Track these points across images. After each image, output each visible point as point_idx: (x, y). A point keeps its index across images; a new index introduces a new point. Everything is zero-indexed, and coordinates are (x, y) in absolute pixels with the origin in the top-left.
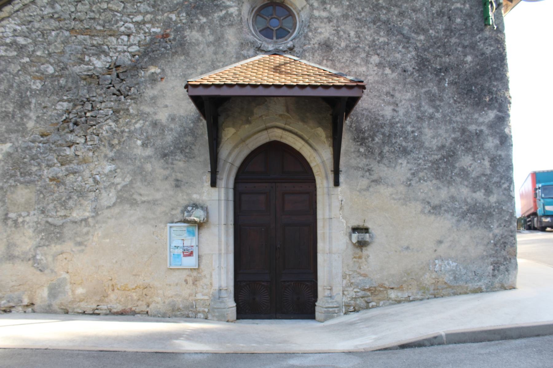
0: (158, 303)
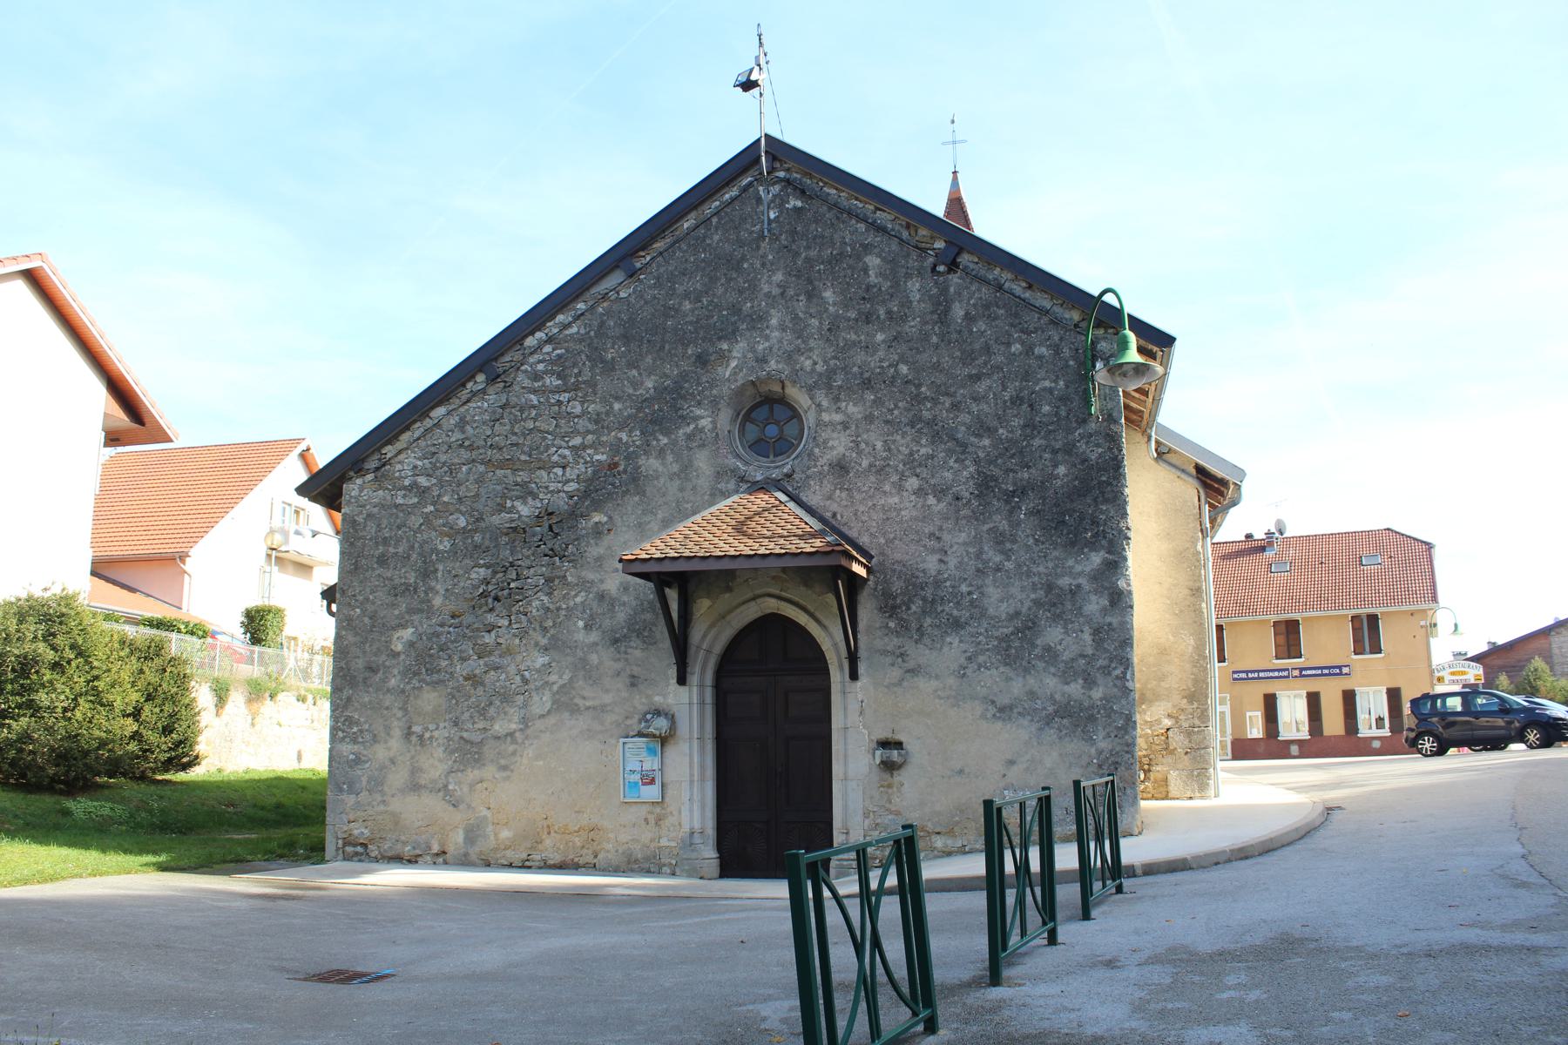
0: (609, 851)
